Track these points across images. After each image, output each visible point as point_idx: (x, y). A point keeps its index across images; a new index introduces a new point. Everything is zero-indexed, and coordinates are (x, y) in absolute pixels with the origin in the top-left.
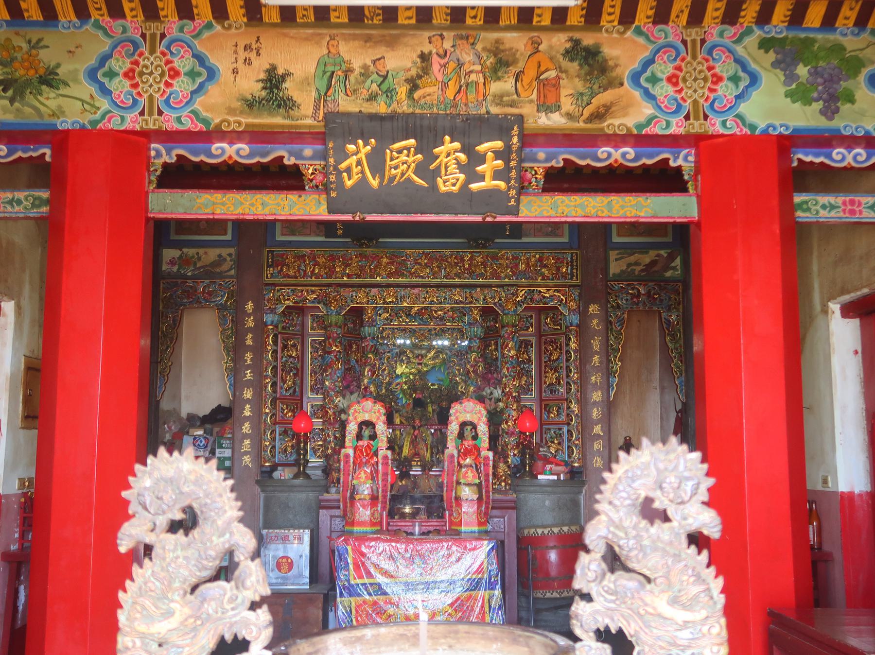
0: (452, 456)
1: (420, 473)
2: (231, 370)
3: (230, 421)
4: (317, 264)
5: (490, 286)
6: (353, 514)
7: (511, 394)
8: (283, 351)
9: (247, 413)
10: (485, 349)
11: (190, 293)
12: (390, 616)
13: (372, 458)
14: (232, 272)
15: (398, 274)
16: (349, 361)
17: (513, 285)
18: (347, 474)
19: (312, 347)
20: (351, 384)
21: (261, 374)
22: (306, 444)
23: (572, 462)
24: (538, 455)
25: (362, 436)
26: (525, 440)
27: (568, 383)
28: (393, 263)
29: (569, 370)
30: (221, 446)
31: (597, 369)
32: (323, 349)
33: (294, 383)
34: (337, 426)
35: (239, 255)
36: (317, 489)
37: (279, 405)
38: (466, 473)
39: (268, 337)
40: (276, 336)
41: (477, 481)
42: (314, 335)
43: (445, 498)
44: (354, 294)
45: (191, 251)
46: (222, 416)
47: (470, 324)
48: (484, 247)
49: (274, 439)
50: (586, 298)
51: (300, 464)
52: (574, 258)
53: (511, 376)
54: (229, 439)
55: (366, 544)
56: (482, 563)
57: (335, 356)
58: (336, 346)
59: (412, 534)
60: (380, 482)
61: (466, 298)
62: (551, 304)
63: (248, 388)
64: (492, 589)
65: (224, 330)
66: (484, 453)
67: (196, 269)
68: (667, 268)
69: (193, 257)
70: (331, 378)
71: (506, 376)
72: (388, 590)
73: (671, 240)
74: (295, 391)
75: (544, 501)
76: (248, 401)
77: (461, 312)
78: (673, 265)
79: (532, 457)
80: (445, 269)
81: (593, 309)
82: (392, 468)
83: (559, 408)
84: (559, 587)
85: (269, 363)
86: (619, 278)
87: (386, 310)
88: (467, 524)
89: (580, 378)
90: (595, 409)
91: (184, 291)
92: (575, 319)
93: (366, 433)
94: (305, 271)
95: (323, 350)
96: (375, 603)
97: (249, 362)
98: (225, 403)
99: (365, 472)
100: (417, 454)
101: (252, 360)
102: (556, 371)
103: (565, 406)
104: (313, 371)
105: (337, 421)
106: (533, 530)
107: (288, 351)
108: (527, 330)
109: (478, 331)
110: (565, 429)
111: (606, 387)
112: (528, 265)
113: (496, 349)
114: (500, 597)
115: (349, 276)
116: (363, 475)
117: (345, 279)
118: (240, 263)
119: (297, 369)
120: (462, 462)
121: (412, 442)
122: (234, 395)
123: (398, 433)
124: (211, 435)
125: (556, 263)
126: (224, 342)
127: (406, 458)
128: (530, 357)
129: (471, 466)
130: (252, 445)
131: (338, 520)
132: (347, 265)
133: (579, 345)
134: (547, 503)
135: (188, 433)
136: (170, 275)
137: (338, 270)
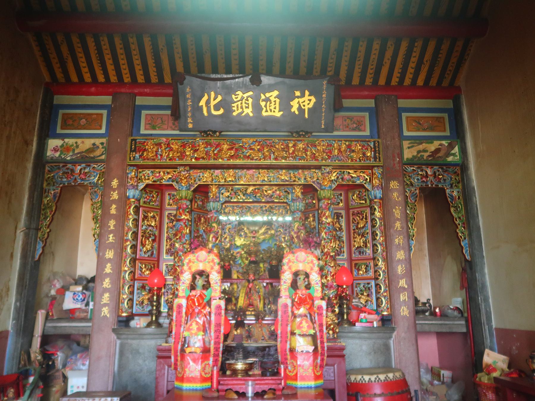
0: (286, 306)
4: (171, 150)
5: (308, 168)
6: (183, 369)
7: (329, 254)
8: (143, 220)
13: (204, 308)
14: (103, 157)
17: (328, 166)
18: (179, 326)
20: (197, 243)
23: (382, 311)
26: (343, 292)
27: (374, 245)
29: (374, 234)
31: (400, 233)
33: (152, 247)
35: (109, 142)
38: (301, 323)
39: (130, 208)
41: (312, 332)
42: (170, 209)
43: (279, 350)
44: (201, 175)
45: (70, 141)
47: (293, 200)
48: (304, 136)
49: (132, 293)
50: (387, 177)
52: (377, 145)
53: (328, 239)
57: (185, 223)
58: (185, 215)
61: (291, 177)
62: (358, 182)
63: (110, 249)
66: (317, 303)
68: (448, 154)
69: (73, 145)
71: (325, 239)
76: (109, 260)
78: (453, 152)
79: (348, 308)
80: (274, 153)
81: (394, 184)
82: (226, 318)
83: (367, 266)
85: (130, 229)
86: (410, 163)
88: (303, 379)
89: (386, 240)
91: (64, 173)
92: (379, 193)
93: (200, 282)
94: (161, 155)
97: (112, 228)
99: (197, 323)
100: (251, 305)
101: (114, 226)
102: (363, 236)
103: (372, 264)
107: (148, 221)
109: (300, 205)
110: (373, 283)
111: (407, 247)
112: (339, 150)
113: (314, 220)
115: (196, 159)
116: (194, 326)
117: (193, 160)
118: (108, 151)
119: (155, 235)
120: (296, 312)
121: (246, 294)
125: (362, 149)
127: (241, 309)
128: (341, 226)
129: (306, 316)
130: (111, 298)
132: (196, 151)
133: (383, 214)
134: (364, 348)
136: (54, 161)
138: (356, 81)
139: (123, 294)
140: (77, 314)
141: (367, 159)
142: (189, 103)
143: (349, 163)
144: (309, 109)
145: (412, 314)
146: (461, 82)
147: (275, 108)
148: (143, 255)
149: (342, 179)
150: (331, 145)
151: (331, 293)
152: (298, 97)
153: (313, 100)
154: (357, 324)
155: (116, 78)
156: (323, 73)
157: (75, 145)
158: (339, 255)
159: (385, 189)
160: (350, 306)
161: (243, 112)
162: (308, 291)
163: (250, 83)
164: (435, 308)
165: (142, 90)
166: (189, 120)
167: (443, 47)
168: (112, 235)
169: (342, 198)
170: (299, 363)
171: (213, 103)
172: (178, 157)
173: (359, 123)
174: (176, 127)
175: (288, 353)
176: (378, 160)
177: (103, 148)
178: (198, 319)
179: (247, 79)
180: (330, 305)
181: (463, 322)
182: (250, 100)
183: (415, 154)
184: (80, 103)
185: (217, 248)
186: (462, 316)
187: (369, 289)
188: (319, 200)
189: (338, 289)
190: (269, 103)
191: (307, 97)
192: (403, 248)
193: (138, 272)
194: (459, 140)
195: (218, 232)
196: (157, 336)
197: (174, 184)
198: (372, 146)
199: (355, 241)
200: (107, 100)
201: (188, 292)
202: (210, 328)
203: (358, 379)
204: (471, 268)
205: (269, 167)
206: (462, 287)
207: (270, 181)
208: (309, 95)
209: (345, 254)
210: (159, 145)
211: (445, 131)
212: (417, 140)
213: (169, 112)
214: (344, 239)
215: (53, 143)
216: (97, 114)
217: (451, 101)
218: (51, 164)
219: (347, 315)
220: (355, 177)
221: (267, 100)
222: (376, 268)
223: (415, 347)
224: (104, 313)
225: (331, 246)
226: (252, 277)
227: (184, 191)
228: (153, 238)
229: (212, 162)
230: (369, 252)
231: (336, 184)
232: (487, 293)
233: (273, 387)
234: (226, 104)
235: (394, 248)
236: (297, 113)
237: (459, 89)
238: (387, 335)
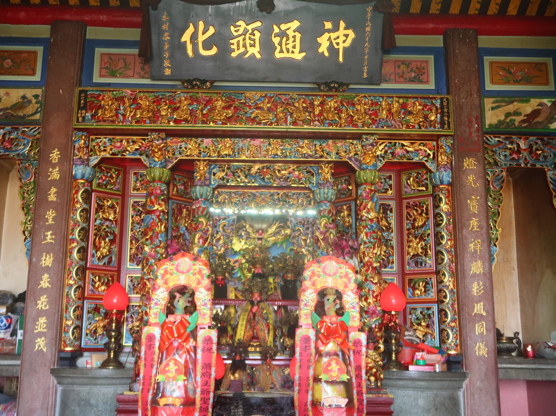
0: (307, 339)
1: (259, 362)
4: (139, 107)
7: (371, 264)
8: (97, 212)
10: (336, 215)
13: (186, 340)
14: (38, 116)
16: (178, 227)
17: (372, 134)
18: (149, 366)
19: (134, 210)
24: (404, 340)
26: (390, 321)
27: (438, 253)
28: (231, 106)
29: (438, 237)
31: (477, 235)
33: (110, 251)
35: (46, 95)
37: (89, 276)
38: (329, 364)
39: (77, 192)
41: (345, 377)
42: (136, 197)
43: (296, 403)
44: (183, 145)
47: (319, 185)
48: (337, 90)
49: (80, 318)
50: (460, 150)
57: (158, 216)
58: (159, 204)
61: (316, 151)
62: (416, 159)
63: (48, 253)
66: (354, 335)
70: (152, 243)
71: (365, 243)
73: (553, 89)
74: (111, 258)
75: (416, 399)
76: (47, 269)
77: (309, 165)
79: (398, 344)
80: (291, 114)
81: (469, 163)
83: (427, 283)
86: (495, 131)
89: (455, 246)
93: (181, 303)
94: (124, 116)
97: (50, 221)
99: (176, 363)
100: (255, 337)
101: (54, 219)
102: (422, 239)
103: (434, 280)
108: (386, 192)
109: (329, 192)
111: (487, 256)
112: (389, 111)
113: (349, 215)
115: (176, 121)
116: (172, 367)
117: (172, 124)
118: (45, 106)
119: (113, 234)
120: (322, 348)
121: (249, 321)
123: (232, 310)
127: (240, 343)
132: (176, 109)
133: (453, 207)
134: (421, 402)
139: (67, 320)
141: (431, 126)
142: (166, 37)
143: (404, 130)
144: (344, 48)
145: (493, 355)
147: (294, 47)
148: (96, 262)
149: (393, 153)
150: (377, 104)
151: (374, 322)
152: (329, 31)
154: (411, 368)
159: (457, 170)
160: (402, 342)
162: (340, 319)
164: (526, 346)
165: (94, 17)
166: (166, 63)
168: (51, 232)
169: (391, 182)
171: (201, 38)
172: (149, 118)
176: (446, 126)
177: (37, 103)
180: (372, 339)
182: (257, 35)
183: (502, 118)
187: (429, 316)
188: (358, 185)
189: (383, 316)
190: (285, 39)
191: (342, 31)
192: (481, 258)
193: (89, 288)
195: (208, 230)
196: (117, 381)
197: (143, 158)
198: (438, 105)
199: (409, 247)
200: (43, 30)
201: (163, 317)
205: (283, 136)
207: (286, 157)
208: (346, 28)
209: (395, 265)
210: (121, 99)
211: (547, 84)
213: (136, 51)
214: (394, 243)
216: (28, 52)
220: (412, 152)
221: (283, 34)
222: (441, 286)
223: (495, 401)
224: (39, 346)
227: (158, 170)
228: (112, 237)
229: (199, 126)
230: (430, 262)
231: (384, 162)
234: (221, 40)
236: (326, 54)
238: (456, 384)
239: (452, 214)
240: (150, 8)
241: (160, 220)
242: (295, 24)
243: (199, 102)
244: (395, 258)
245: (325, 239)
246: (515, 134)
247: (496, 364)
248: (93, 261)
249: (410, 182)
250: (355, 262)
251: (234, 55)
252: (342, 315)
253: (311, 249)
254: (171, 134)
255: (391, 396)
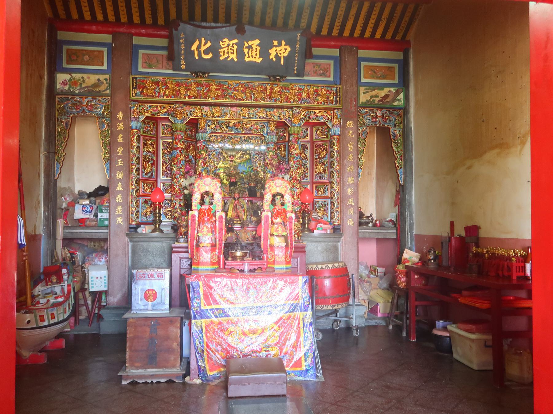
2: (108, 160)
3: (107, 195)
4: (167, 88)
5: (283, 107)
6: (199, 257)
9: (119, 188)
11: (77, 105)
12: (231, 332)
13: (211, 217)
14: (108, 92)
15: (224, 96)
16: (188, 156)
17: (298, 107)
19: (163, 146)
20: (191, 170)
21: (129, 162)
22: (160, 210)
25: (204, 202)
26: (305, 208)
27: (331, 172)
29: (332, 163)
30: (101, 211)
32: (170, 147)
33: (152, 170)
34: (182, 198)
35: (112, 79)
36: (169, 239)
37: (141, 184)
38: (278, 228)
39: (133, 137)
40: (139, 136)
41: (285, 234)
42: (164, 138)
45: (78, 76)
46: (102, 192)
48: (280, 81)
49: (138, 206)
50: (345, 117)
51: (156, 224)
54: (107, 206)
55: (213, 279)
56: (298, 293)
57: (180, 151)
58: (181, 144)
59: (242, 271)
60: (217, 235)
61: (267, 115)
62: (322, 121)
63: (120, 171)
64: (306, 311)
65: (102, 131)
66: (289, 215)
67: (81, 88)
68: (394, 100)
69: (80, 80)
70: (177, 166)
71: (293, 167)
72: (230, 313)
75: (317, 247)
77: (263, 123)
79: (309, 220)
81: (350, 124)
84: (332, 303)
85: (134, 155)
86: (364, 106)
87: (213, 123)
88: (278, 263)
89: (340, 169)
90: (349, 189)
91: (73, 104)
92: (337, 131)
93: (207, 200)
94: (159, 93)
95: (171, 148)
96: (220, 323)
97: (120, 154)
98: (104, 184)
101: (122, 152)
102: (323, 164)
104: (164, 163)
105: (181, 195)
106: (315, 266)
107: (147, 147)
109: (274, 138)
110: (328, 201)
112: (308, 94)
113: (284, 150)
114: (311, 316)
115: (189, 97)
116: (205, 229)
117: (187, 98)
118: (112, 86)
120: (275, 221)
121: (234, 208)
122: (110, 177)
124: (95, 204)
126: (102, 140)
129: (281, 223)
130: (123, 211)
131: (185, 260)
132: (189, 90)
133: (340, 148)
134: (319, 248)
135: (78, 203)
136: (63, 93)
137: (182, 92)
138: (324, 32)
140: (88, 223)
141: (330, 102)
142: (183, 47)
143: (316, 105)
144: (284, 56)
145: (357, 224)
146: (411, 37)
147: (256, 55)
148: (145, 176)
149: (309, 117)
150: (301, 89)
151: (297, 208)
152: (276, 46)
153: (289, 49)
154: (315, 231)
155: (114, 17)
156: (297, 27)
157: (82, 80)
158: (303, 179)
159: (343, 127)
160: (311, 219)
161: (228, 57)
162: (283, 207)
163: (236, 32)
164: (376, 221)
165: (138, 31)
166: (182, 62)
167: (398, 8)
169: (308, 132)
170: (276, 253)
171: (203, 48)
172: (174, 95)
173: (326, 69)
174: (170, 66)
175: (269, 247)
177: (107, 83)
178: (207, 225)
179: (234, 28)
180: (297, 217)
181: (395, 231)
182: (235, 47)
184: (82, 40)
185: (205, 171)
186: (395, 226)
187: (325, 205)
188: (290, 135)
189: (302, 205)
190: (251, 50)
191: (283, 46)
192: (353, 175)
193: (141, 190)
194: (404, 88)
195: (206, 158)
196: (163, 239)
197: (170, 117)
198: (335, 91)
199: (316, 168)
200: (107, 38)
201: (199, 207)
202: (216, 232)
203: (314, 268)
204: (403, 191)
205: (249, 106)
206: (395, 205)
207: (250, 118)
208: (285, 45)
209: (308, 178)
210: (157, 83)
211: (394, 79)
212: (371, 86)
213: (165, 53)
214: (308, 166)
215: (61, 77)
216: (98, 51)
217: (402, 53)
218: (62, 96)
219: (308, 225)
221: (250, 47)
222: (332, 190)
223: (356, 248)
225: (297, 172)
226: (237, 196)
227: (180, 124)
229: (203, 100)
230: (327, 177)
231: (304, 122)
232: (412, 209)
233: (261, 266)
234: (214, 50)
235: (346, 175)
236: (274, 59)
237: (408, 42)
238: (337, 239)
239: (339, 152)
240: (174, 30)
241: (181, 153)
242: (257, 42)
243: (202, 85)
244: (309, 174)
245: (271, 164)
246: (374, 108)
247: (358, 230)
248: (143, 175)
249: (318, 134)
250: (287, 177)
251: (222, 58)
252: (284, 205)
253: (263, 169)
254: (186, 104)
255: (305, 243)
